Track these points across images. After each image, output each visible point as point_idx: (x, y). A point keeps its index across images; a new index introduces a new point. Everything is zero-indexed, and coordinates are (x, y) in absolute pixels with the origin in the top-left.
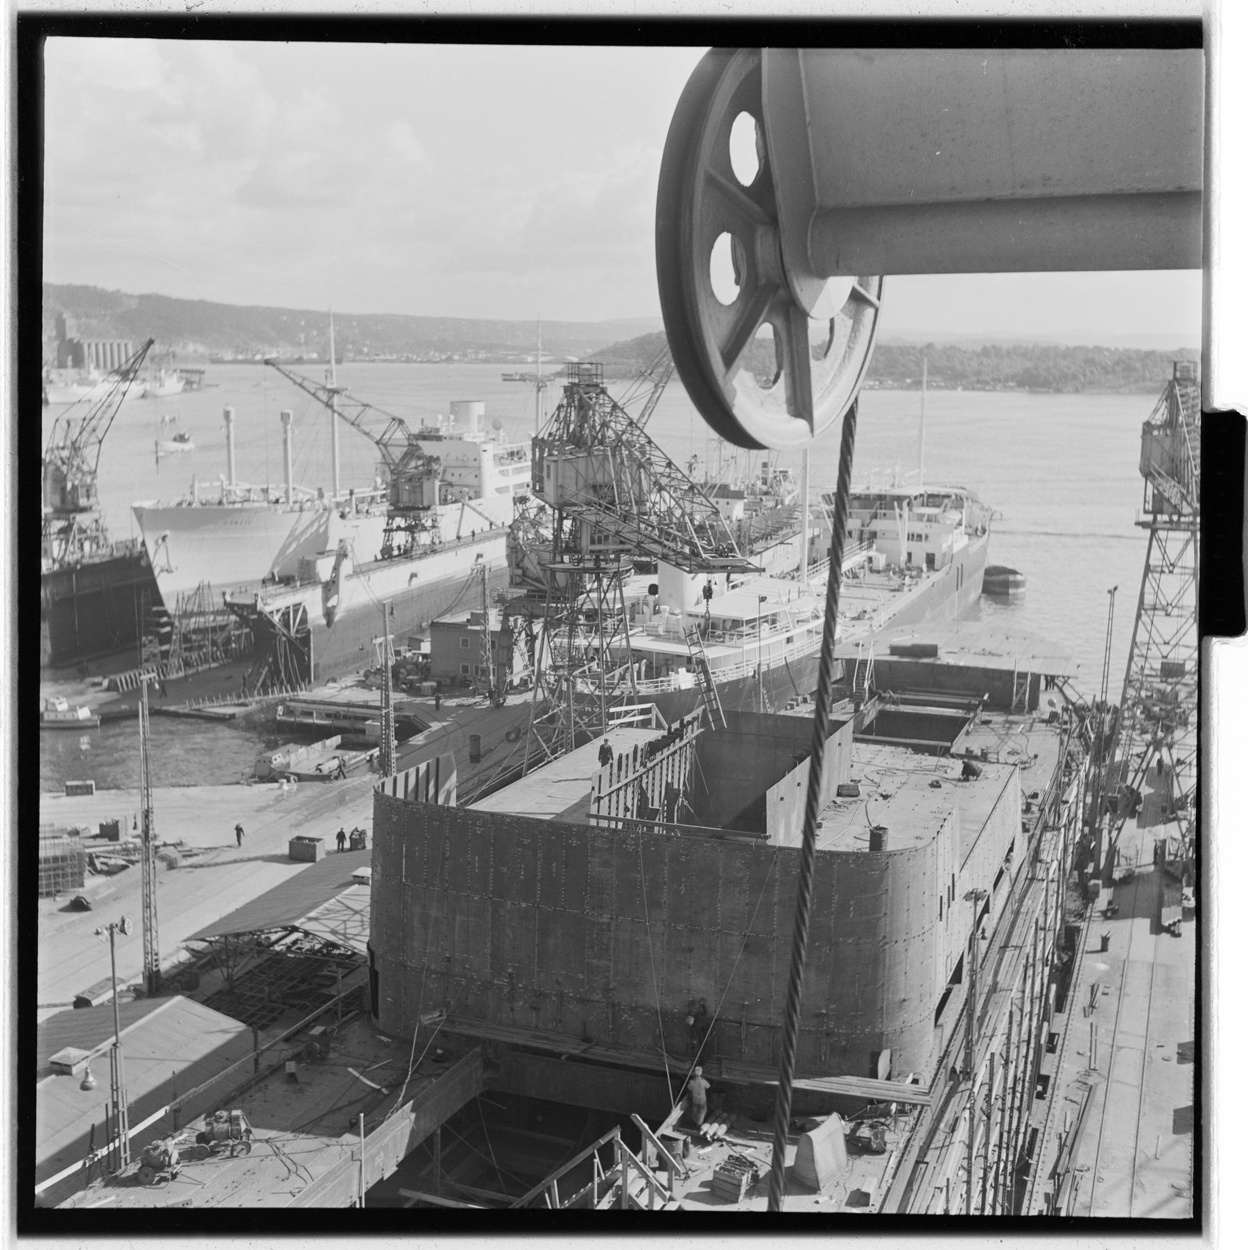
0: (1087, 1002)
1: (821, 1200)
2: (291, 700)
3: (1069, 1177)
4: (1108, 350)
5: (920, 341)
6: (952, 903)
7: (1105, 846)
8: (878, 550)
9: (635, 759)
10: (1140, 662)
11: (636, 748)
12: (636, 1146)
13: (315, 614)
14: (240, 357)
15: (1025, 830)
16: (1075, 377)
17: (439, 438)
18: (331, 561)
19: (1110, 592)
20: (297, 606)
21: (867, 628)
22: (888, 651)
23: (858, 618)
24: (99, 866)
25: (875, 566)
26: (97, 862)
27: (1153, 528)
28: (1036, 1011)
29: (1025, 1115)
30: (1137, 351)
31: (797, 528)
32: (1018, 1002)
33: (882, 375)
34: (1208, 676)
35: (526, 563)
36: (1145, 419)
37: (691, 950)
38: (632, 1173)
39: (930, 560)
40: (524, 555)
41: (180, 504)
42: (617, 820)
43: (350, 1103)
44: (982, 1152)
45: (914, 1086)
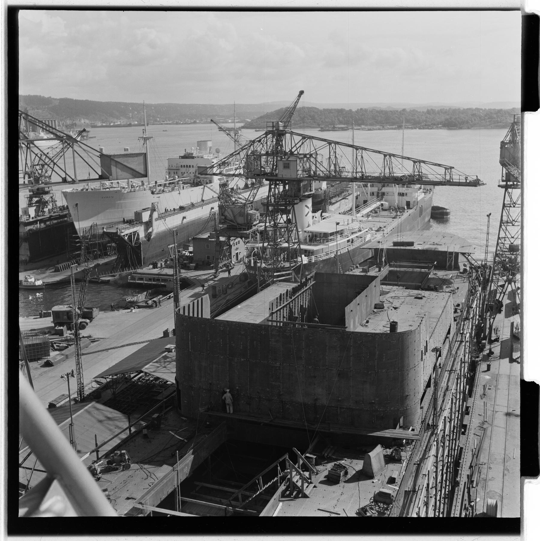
0: (482, 392)
1: (374, 481)
2: (134, 273)
3: (477, 467)
4: (481, 109)
5: (400, 108)
6: (427, 353)
7: (488, 326)
8: (386, 201)
9: (287, 296)
10: (501, 245)
11: (287, 290)
12: (295, 461)
13: (142, 235)
14: (104, 124)
15: (455, 320)
16: (467, 122)
17: (193, 158)
18: (149, 213)
19: (488, 216)
20: (135, 232)
21: (382, 235)
22: (392, 245)
23: (378, 231)
24: (56, 348)
25: (384, 207)
26: (55, 345)
27: (506, 187)
28: (461, 398)
29: (458, 442)
30: (494, 109)
31: (350, 192)
32: (455, 395)
33: (383, 124)
35: (226, 213)
36: (502, 140)
37: (315, 377)
38: (294, 473)
39: (408, 204)
40: (225, 210)
41: (82, 190)
42: (280, 322)
43: (171, 446)
44: (441, 459)
45: (412, 432)
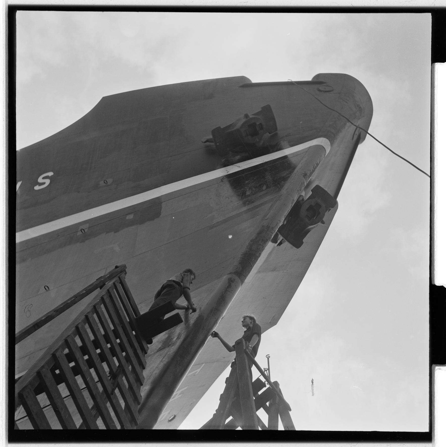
34: (434, 242)
